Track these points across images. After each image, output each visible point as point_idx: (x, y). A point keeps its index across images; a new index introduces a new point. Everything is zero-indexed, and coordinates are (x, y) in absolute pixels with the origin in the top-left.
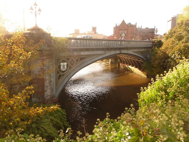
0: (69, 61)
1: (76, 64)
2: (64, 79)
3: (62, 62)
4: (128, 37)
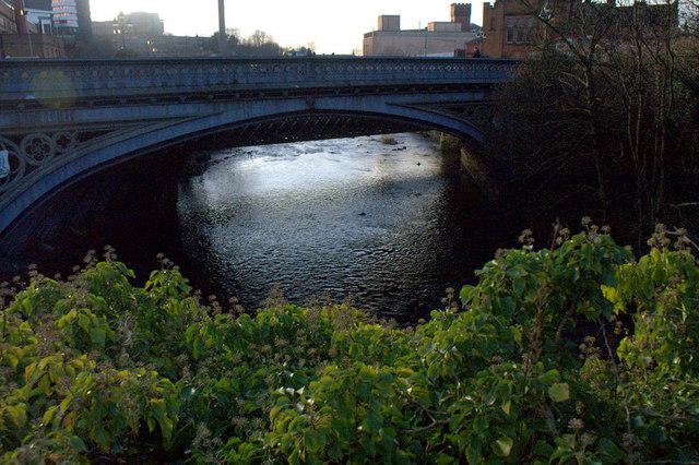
0: (18, 144)
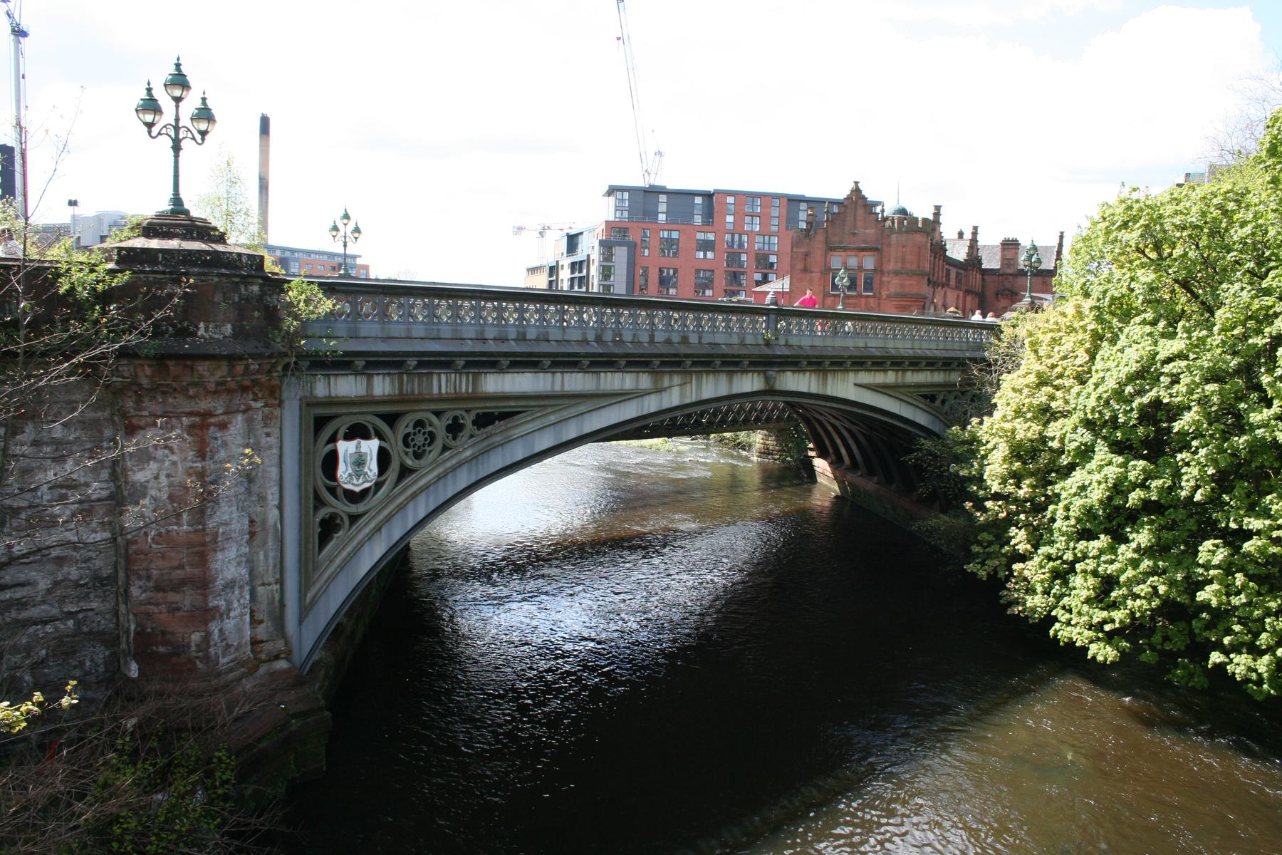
1: (445, 448)
2: (361, 545)
3: (348, 437)
4: (884, 293)
